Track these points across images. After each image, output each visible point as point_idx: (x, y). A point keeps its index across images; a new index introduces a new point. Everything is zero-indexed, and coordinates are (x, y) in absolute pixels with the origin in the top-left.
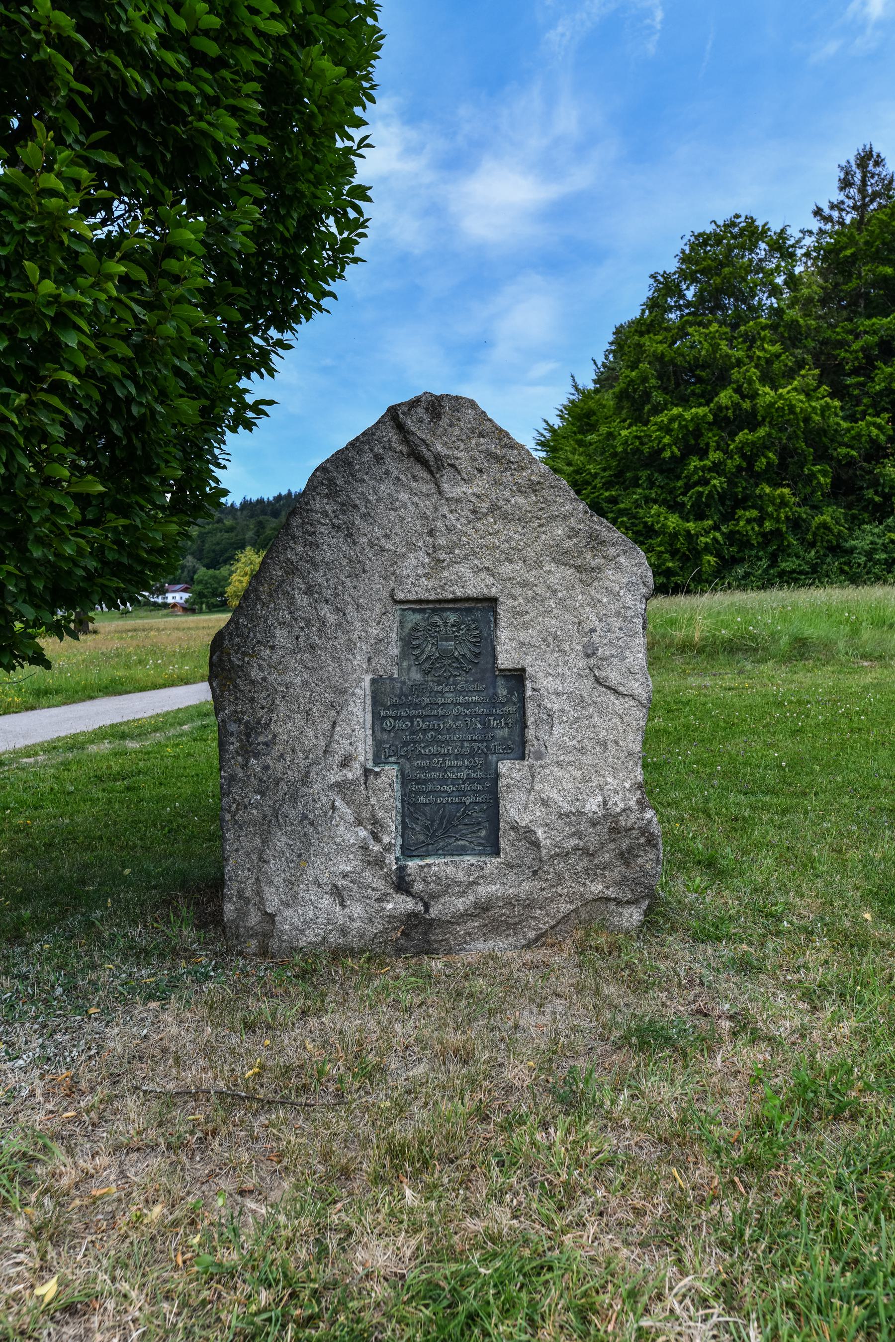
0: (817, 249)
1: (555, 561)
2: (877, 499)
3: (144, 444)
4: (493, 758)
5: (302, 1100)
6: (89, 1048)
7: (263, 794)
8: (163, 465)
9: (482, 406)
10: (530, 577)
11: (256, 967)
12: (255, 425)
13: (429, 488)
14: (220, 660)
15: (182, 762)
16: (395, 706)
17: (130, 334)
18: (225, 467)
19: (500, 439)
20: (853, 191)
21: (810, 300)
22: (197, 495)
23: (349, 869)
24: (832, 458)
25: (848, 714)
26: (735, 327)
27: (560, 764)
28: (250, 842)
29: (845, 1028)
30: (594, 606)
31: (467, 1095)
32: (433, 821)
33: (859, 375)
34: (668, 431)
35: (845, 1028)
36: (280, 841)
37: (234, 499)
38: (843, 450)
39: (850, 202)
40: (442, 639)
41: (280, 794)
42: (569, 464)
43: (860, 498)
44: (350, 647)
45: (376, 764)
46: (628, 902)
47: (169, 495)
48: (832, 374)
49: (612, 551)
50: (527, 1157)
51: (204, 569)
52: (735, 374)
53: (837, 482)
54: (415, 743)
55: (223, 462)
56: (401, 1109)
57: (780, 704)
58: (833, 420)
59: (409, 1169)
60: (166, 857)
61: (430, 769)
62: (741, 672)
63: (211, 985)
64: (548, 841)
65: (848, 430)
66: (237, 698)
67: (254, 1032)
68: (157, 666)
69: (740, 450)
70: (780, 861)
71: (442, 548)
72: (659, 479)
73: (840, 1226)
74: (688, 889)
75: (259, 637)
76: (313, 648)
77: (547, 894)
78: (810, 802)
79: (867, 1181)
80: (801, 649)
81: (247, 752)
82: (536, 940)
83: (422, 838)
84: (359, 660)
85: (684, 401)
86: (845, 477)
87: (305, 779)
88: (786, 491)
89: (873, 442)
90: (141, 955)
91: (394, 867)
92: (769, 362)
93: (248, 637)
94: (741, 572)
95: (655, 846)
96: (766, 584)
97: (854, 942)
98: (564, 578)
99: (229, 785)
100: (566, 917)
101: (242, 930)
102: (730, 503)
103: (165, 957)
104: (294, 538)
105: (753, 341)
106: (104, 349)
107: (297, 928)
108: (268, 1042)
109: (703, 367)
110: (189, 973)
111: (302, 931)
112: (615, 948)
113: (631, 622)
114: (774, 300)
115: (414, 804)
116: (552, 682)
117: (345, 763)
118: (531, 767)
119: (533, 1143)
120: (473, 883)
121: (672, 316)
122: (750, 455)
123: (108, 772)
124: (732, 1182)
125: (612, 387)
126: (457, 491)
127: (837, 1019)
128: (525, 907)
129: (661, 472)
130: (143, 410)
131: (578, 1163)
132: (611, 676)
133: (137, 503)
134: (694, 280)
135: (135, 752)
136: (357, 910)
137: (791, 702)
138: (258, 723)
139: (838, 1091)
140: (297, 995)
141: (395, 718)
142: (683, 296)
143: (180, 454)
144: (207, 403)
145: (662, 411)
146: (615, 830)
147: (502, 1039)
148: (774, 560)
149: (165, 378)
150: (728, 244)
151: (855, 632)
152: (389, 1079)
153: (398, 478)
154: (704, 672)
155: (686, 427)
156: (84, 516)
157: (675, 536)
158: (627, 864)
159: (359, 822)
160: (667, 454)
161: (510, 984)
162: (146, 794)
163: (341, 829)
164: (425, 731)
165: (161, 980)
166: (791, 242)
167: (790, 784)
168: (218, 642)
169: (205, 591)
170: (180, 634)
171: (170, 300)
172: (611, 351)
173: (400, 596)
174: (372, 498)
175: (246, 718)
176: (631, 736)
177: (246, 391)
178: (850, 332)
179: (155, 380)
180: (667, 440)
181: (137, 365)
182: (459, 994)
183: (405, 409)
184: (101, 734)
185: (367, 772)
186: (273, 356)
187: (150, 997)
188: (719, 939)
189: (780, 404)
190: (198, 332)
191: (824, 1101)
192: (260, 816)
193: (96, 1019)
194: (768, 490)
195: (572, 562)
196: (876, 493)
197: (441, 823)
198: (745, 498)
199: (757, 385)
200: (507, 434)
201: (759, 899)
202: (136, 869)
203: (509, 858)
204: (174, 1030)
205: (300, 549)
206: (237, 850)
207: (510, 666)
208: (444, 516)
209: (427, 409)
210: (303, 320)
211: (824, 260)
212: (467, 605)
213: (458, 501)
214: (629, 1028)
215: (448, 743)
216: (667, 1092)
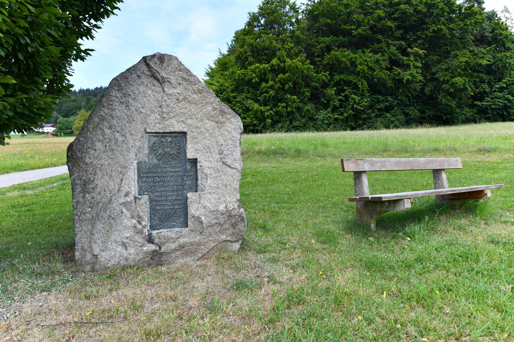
0: (306, 10)
2: (325, 101)
3: (34, 64)
4: (185, 192)
5: (111, 321)
6: (15, 313)
7: (92, 208)
8: (43, 73)
9: (180, 59)
11: (90, 276)
12: (85, 59)
13: (160, 89)
14: (72, 155)
15: (54, 199)
16: (147, 173)
17: (26, 16)
18: (72, 75)
19: (187, 73)
21: (304, 29)
22: (59, 87)
23: (129, 235)
24: (310, 86)
25: (312, 176)
26: (278, 36)
27: (210, 193)
28: (86, 227)
29: (303, 277)
30: (222, 136)
31: (175, 311)
32: (162, 216)
33: (319, 57)
34: (255, 72)
35: (303, 277)
36: (100, 226)
37: (76, 88)
38: (314, 84)
40: (165, 147)
41: (99, 208)
42: (218, 82)
43: (320, 101)
44: (128, 150)
45: (139, 195)
46: (235, 241)
47: (46, 86)
48: (310, 56)
49: (229, 116)
50: (196, 329)
51: (62, 118)
52: (278, 53)
53: (312, 95)
54: (155, 187)
55: (71, 73)
56: (149, 319)
57: (291, 173)
58: (311, 73)
59: (152, 339)
60: (48, 237)
61: (161, 196)
62: (278, 161)
63: (70, 284)
64: (206, 221)
65: (316, 77)
66: (79, 170)
67: (90, 299)
68: (40, 159)
69: (280, 81)
70: (287, 225)
71: (165, 113)
72: (251, 90)
73: (296, 336)
74: (257, 237)
75: (89, 145)
76: (112, 150)
77: (206, 240)
78: (298, 205)
79: (306, 321)
80: (298, 153)
81: (84, 192)
82: (202, 257)
83: (158, 222)
84: (132, 155)
85: (260, 62)
86: (315, 93)
87: (110, 201)
88: (295, 97)
89: (324, 81)
90: (39, 275)
91: (147, 234)
92: (290, 50)
93: (84, 145)
94: (280, 126)
95: (244, 221)
96: (288, 131)
97: (307, 250)
98: (211, 126)
99: (77, 205)
100: (213, 248)
101: (83, 262)
102: (276, 100)
103: (49, 275)
104: (103, 106)
105: (284, 42)
106: (14, 22)
107: (107, 260)
108: (95, 302)
109: (267, 49)
110: (60, 280)
112: (230, 258)
113: (235, 142)
114: (292, 27)
115: (155, 210)
117: (127, 195)
118: (199, 194)
119: (198, 324)
120: (178, 238)
121: (256, 29)
122: (283, 83)
123: (18, 204)
124: (265, 328)
125: (234, 54)
126: (171, 91)
127: (301, 274)
128: (197, 246)
129: (252, 87)
130: (34, 50)
131: (214, 329)
132: (228, 161)
133: (31, 88)
134: (264, 17)
135: (31, 195)
136: (132, 251)
137: (294, 172)
138: (89, 180)
139: (299, 296)
140: (108, 284)
141: (147, 177)
142: (260, 22)
143: (51, 69)
144: (62, 48)
145: (252, 65)
146: (230, 216)
147: (188, 292)
148: (291, 121)
149: (44, 37)
150: (276, 5)
151: (316, 148)
152: (145, 310)
153: (147, 85)
154: (266, 162)
155: (261, 71)
156: (6, 93)
157: (257, 111)
158: (234, 228)
159: (133, 217)
160: (254, 81)
161: (191, 273)
162: (37, 212)
163: (125, 220)
164: (159, 182)
165: (47, 284)
166: (297, 7)
167: (292, 200)
168: (70, 148)
169: (63, 127)
170: (51, 145)
171: (45, 4)
172: (234, 40)
173: (148, 131)
174: (137, 92)
176: (235, 183)
177: (80, 44)
178: (317, 42)
179: (39, 37)
180: (254, 75)
181: (30, 30)
182: (172, 278)
183: (150, 58)
184: (13, 188)
185: (136, 198)
186: (93, 31)
187: (43, 291)
188: (266, 252)
190: (58, 19)
191: (295, 300)
192: (91, 217)
193: (18, 301)
194: (289, 96)
195: (214, 120)
196: (325, 99)
197: (165, 216)
198: (281, 99)
199: (285, 58)
200: (190, 71)
201: (279, 238)
202: (34, 242)
203: (191, 228)
204: (54, 302)
205: (106, 111)
206: (81, 231)
207: (192, 158)
208: (166, 101)
209: (158, 59)
210: (106, 17)
211: (308, 14)
212: (175, 135)
213: (171, 95)
214: (233, 283)
215: (168, 186)
216: (245, 302)
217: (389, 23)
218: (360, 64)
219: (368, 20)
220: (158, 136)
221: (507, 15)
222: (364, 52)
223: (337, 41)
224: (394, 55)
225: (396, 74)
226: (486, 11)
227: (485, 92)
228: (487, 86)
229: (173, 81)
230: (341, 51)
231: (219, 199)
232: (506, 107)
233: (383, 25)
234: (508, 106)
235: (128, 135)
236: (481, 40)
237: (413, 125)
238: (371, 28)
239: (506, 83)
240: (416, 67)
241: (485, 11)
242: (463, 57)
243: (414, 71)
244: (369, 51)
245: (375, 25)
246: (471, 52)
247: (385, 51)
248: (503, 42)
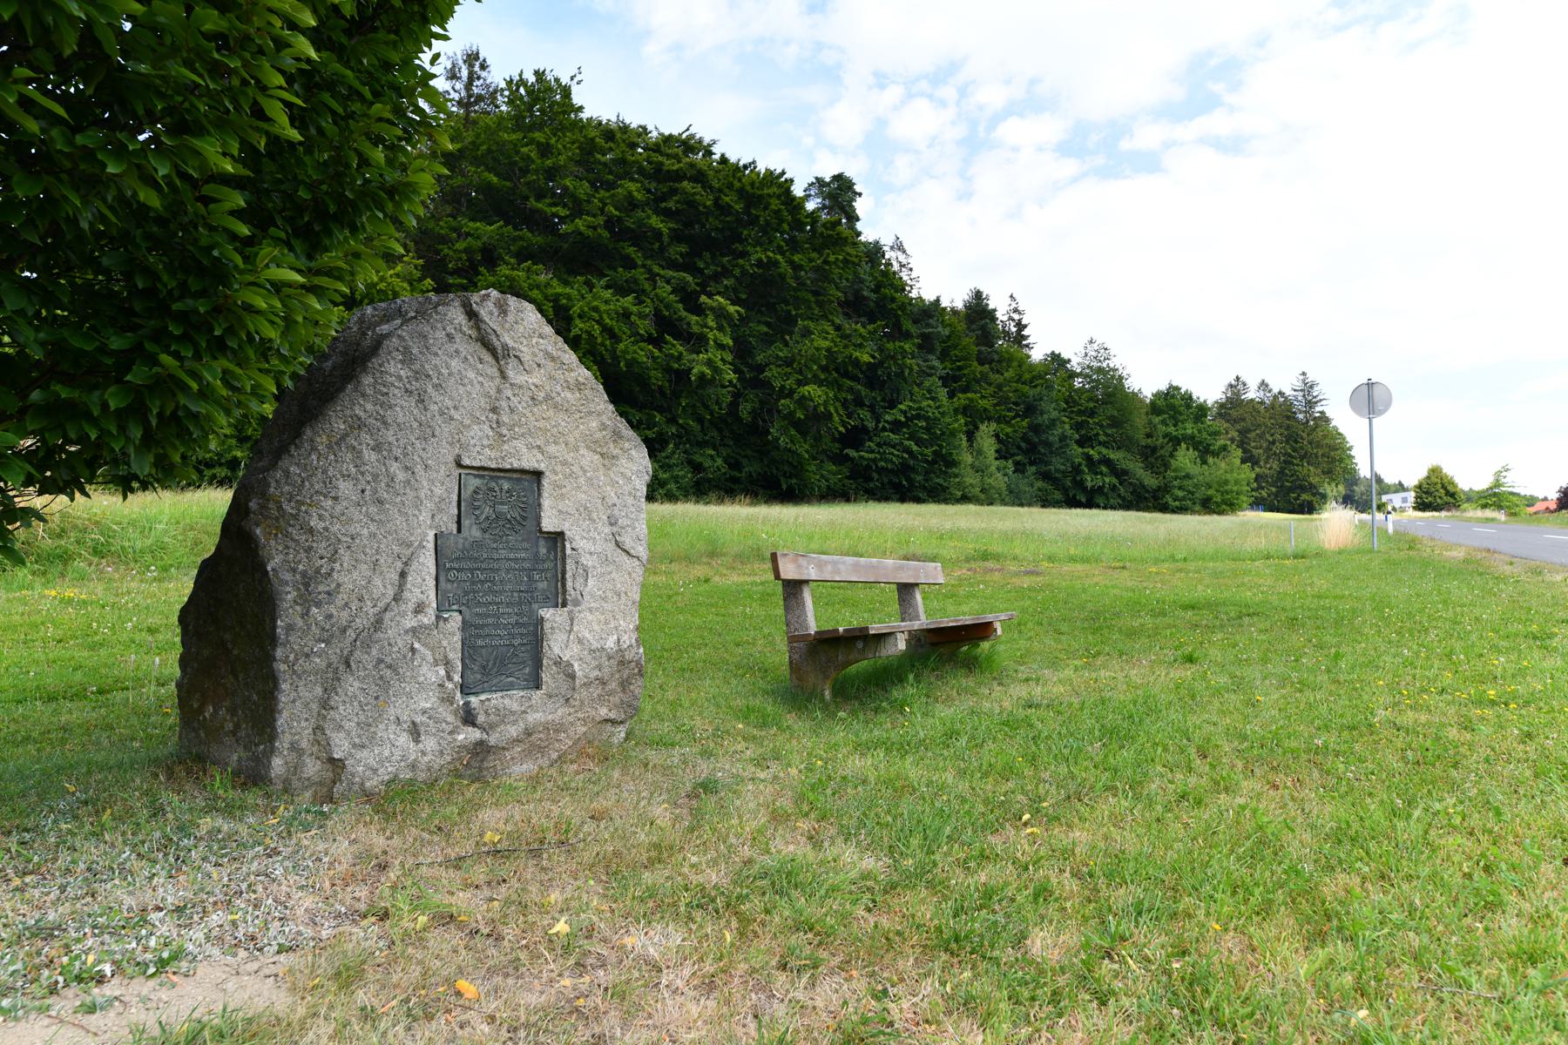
1: (588, 447)
4: (535, 606)
7: (327, 642)
10: (569, 457)
13: (494, 371)
20: (458, 86)
27: (590, 610)
33: (460, 276)
36: (352, 685)
39: (456, 96)
61: (487, 616)
66: (287, 547)
77: (571, 719)
81: (306, 601)
84: (424, 517)
87: (378, 623)
104: (363, 395)
111: (375, 771)
116: (585, 543)
118: (570, 612)
126: (521, 379)
138: (318, 571)
163: (424, 669)
173: (466, 462)
174: (445, 371)
175: (301, 567)
178: (454, 230)
189: (382, 286)
205: (369, 407)
206: (294, 701)
213: (520, 387)
217: (655, 221)
218: (580, 317)
219: (601, 200)
220: (482, 477)
221: (902, 258)
222: (590, 286)
223: (514, 240)
224: (668, 307)
225: (672, 356)
226: (862, 238)
227: (865, 430)
228: (868, 415)
229: (526, 358)
230: (529, 270)
231: (606, 623)
232: (905, 469)
233: (640, 223)
234: (908, 466)
235: (419, 469)
236: (855, 306)
237: (713, 496)
238: (610, 223)
239: (904, 412)
240: (721, 347)
241: (582, 115)
242: (821, 340)
243: (716, 356)
244: (603, 282)
245: (619, 219)
246: (838, 328)
247: (644, 291)
248: (897, 317)
